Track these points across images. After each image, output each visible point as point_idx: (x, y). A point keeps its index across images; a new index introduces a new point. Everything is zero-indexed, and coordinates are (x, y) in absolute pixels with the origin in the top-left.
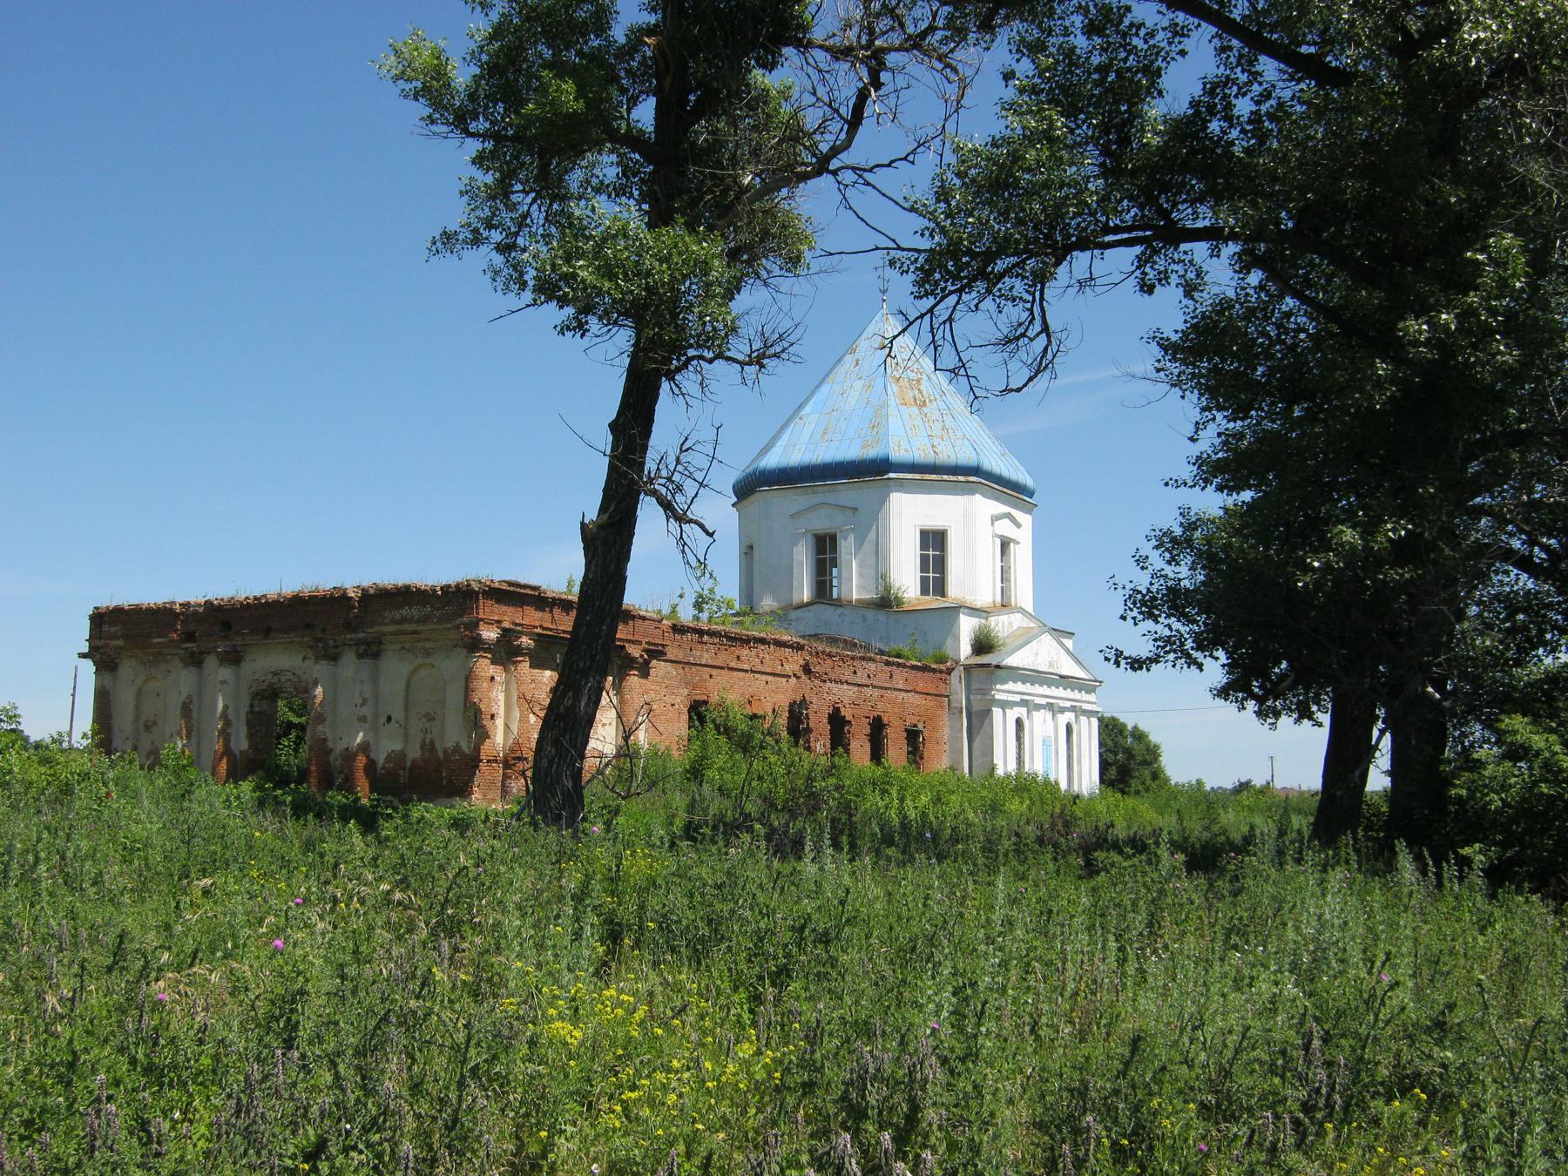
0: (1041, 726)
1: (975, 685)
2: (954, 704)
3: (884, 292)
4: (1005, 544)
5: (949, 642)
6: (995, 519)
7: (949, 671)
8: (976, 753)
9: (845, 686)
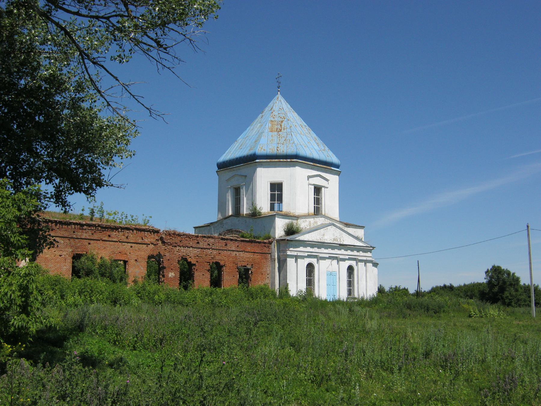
0: (323, 268)
1: (281, 249)
2: (273, 257)
3: (279, 87)
4: (318, 190)
5: (272, 230)
6: (309, 177)
7: (270, 243)
8: (281, 278)
9: (191, 249)
